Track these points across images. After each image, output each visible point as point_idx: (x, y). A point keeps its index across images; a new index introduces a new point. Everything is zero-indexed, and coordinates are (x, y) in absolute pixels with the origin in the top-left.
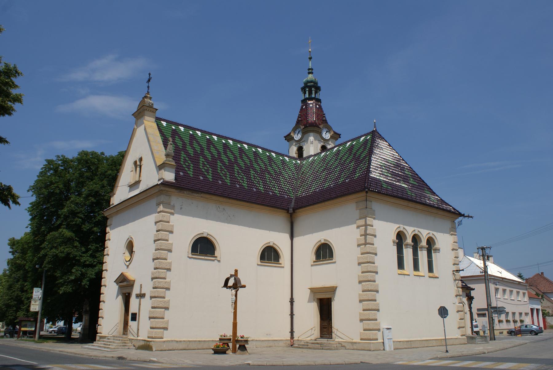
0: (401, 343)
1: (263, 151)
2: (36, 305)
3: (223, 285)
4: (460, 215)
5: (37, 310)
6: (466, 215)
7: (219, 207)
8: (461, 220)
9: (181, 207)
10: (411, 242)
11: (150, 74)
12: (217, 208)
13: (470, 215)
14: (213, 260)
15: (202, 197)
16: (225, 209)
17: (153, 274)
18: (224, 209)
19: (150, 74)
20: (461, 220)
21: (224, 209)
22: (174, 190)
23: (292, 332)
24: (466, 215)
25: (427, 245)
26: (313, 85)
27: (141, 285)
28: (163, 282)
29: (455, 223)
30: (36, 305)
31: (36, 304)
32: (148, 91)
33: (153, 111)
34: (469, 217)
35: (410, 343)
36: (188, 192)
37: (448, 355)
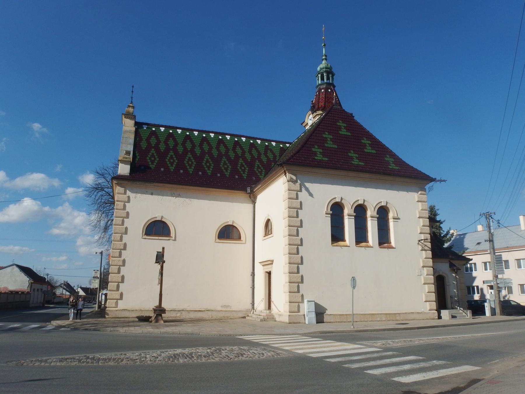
0: (332, 316)
1: (277, 143)
2: (95, 283)
3: (155, 262)
4: (433, 180)
5: (96, 287)
6: (437, 179)
7: (174, 193)
8: (433, 186)
9: (135, 196)
10: (376, 214)
11: (133, 87)
12: (172, 194)
13: (442, 179)
14: (169, 240)
15: (155, 186)
16: (180, 195)
17: (272, 268)
18: (179, 195)
19: (133, 87)
20: (433, 186)
21: (179, 195)
22: (126, 182)
23: (253, 304)
24: (437, 179)
25: (377, 214)
26: (329, 71)
27: (354, 279)
28: (116, 260)
29: (425, 189)
30: (95, 283)
31: (96, 282)
32: (132, 101)
33: (132, 118)
34: (441, 181)
35: (345, 316)
36: (140, 183)
37: (322, 327)
